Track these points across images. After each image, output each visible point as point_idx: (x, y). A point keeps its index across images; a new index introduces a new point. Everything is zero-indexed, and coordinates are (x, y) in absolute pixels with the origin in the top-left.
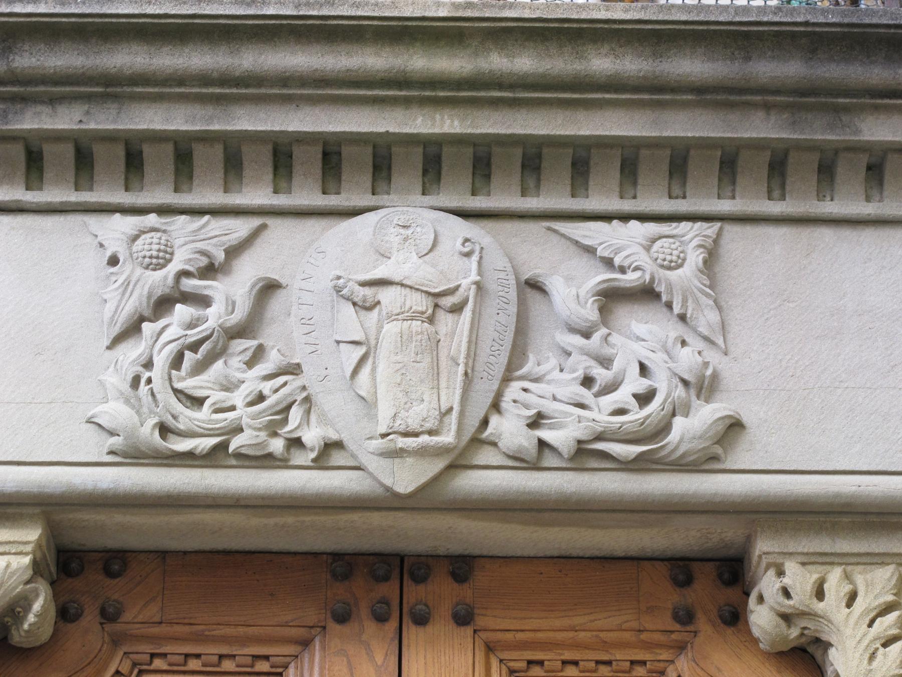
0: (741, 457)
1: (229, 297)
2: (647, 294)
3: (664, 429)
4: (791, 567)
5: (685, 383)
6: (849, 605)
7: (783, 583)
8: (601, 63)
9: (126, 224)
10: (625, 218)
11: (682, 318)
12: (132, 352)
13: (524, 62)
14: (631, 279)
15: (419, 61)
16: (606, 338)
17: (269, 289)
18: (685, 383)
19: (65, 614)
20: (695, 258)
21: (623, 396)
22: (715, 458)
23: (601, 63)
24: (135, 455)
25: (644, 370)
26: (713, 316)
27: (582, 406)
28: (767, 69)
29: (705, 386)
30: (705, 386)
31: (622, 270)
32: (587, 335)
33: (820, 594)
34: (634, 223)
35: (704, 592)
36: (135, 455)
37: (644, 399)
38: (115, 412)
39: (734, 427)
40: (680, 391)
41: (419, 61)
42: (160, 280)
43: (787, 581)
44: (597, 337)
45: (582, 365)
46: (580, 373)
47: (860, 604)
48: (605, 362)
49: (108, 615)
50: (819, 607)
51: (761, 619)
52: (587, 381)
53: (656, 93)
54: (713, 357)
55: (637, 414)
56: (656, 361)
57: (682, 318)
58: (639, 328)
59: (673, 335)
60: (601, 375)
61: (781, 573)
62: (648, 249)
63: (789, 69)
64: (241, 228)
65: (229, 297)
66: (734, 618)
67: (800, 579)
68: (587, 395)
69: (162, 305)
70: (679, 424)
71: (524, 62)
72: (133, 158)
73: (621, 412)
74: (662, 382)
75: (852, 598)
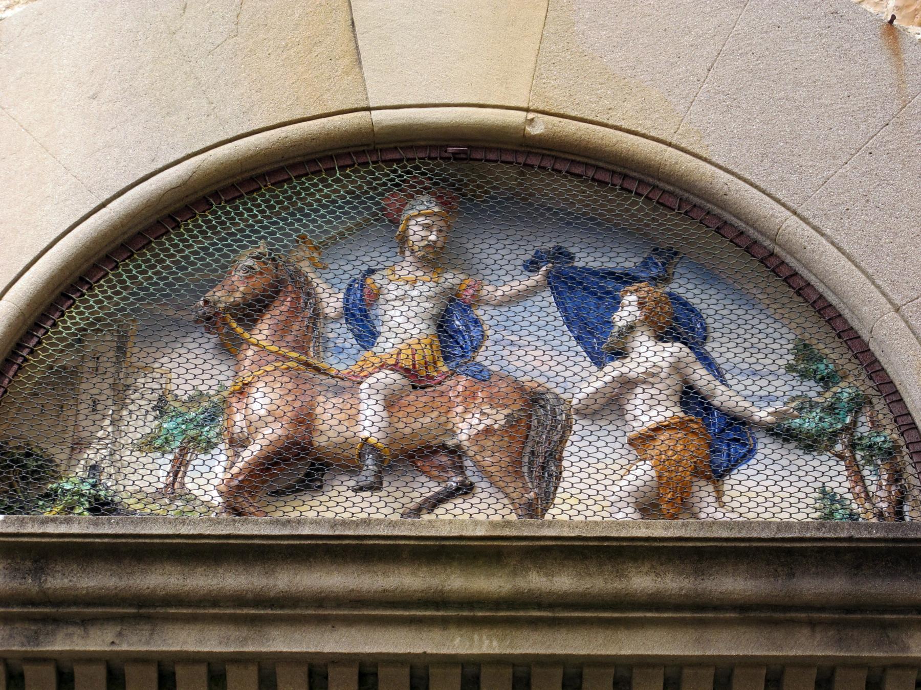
8: (642, 581)
13: (563, 581)
15: (457, 581)
23: (642, 581)
28: (811, 586)
41: (457, 581)
53: (698, 612)
63: (834, 586)
71: (563, 581)
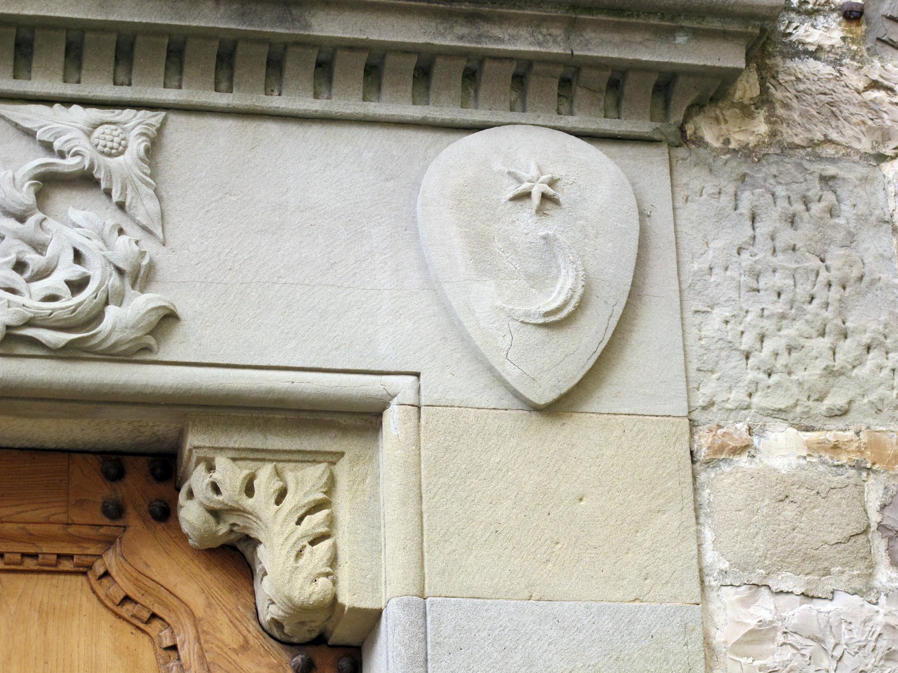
0: (175, 347)
2: (86, 180)
3: (97, 317)
4: (222, 462)
5: (120, 272)
6: (278, 502)
7: (214, 479)
10: (67, 102)
11: (121, 206)
14: (70, 164)
16: (41, 223)
18: (120, 272)
20: (137, 146)
21: (56, 282)
22: (147, 349)
25: (78, 257)
26: (152, 206)
27: (13, 291)
29: (140, 276)
30: (140, 276)
31: (62, 155)
32: (22, 219)
33: (249, 490)
34: (76, 108)
35: (136, 487)
37: (77, 286)
39: (168, 319)
40: (114, 280)
43: (216, 476)
44: (31, 221)
45: (16, 249)
46: (12, 258)
47: (289, 501)
48: (39, 247)
50: (248, 503)
51: (191, 514)
52: (20, 266)
54: (151, 248)
55: (69, 302)
56: (91, 248)
57: (121, 206)
58: (76, 215)
59: (110, 222)
60: (34, 260)
61: (211, 468)
62: (89, 134)
66: (165, 513)
67: (229, 474)
68: (18, 280)
70: (112, 313)
73: (53, 298)
74: (96, 270)
75: (281, 495)
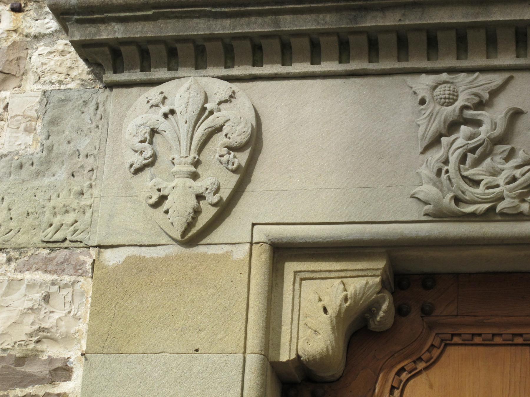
1: (493, 120)
9: (427, 80)
12: (435, 156)
17: (516, 114)
19: (400, 311)
24: (440, 215)
36: (440, 215)
38: (427, 190)
42: (450, 111)
49: (426, 311)
64: (497, 79)
65: (493, 120)
69: (452, 127)
72: (431, 41)
